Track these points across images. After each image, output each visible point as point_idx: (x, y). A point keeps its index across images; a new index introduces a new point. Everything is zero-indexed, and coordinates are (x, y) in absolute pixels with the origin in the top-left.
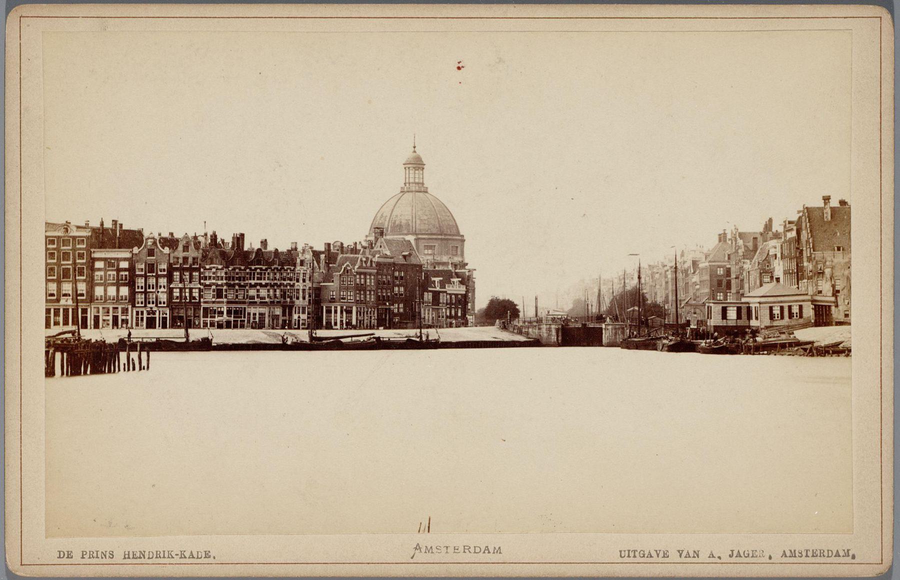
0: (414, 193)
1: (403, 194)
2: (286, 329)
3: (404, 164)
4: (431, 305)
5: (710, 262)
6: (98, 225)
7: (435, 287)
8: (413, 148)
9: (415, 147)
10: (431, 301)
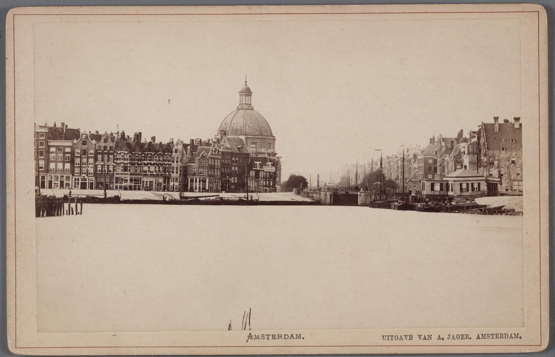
3: (239, 93)
5: (424, 155)
9: (246, 82)
10: (254, 176)
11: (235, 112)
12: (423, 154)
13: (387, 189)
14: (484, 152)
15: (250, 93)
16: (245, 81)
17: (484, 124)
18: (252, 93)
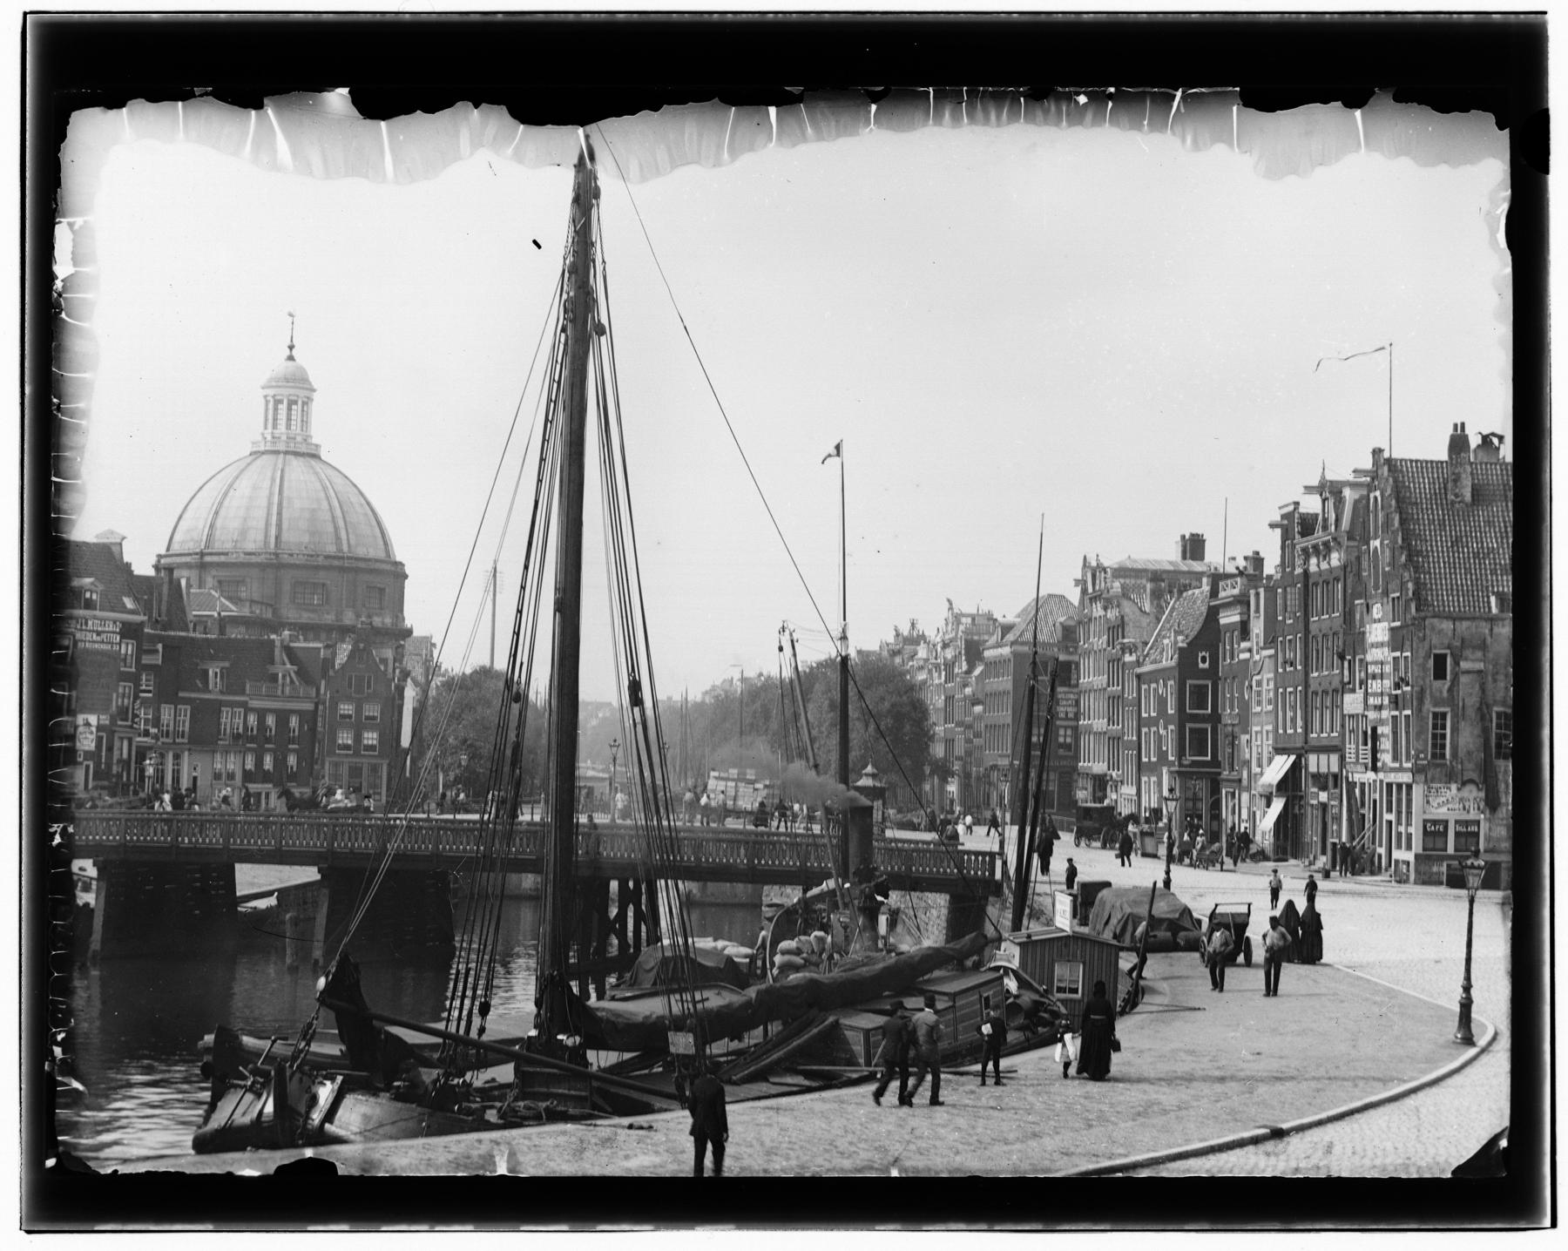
0: (282, 456)
1: (255, 459)
2: (1239, 966)
3: (263, 388)
4: (186, 741)
5: (1013, 643)
6: (1278, 531)
7: (206, 689)
8: (288, 350)
9: (291, 348)
10: (187, 729)
11: (242, 464)
12: (1010, 637)
13: (884, 1043)
14: (121, 754)
15: (307, 389)
16: (289, 343)
17: (1389, 461)
18: (314, 390)
